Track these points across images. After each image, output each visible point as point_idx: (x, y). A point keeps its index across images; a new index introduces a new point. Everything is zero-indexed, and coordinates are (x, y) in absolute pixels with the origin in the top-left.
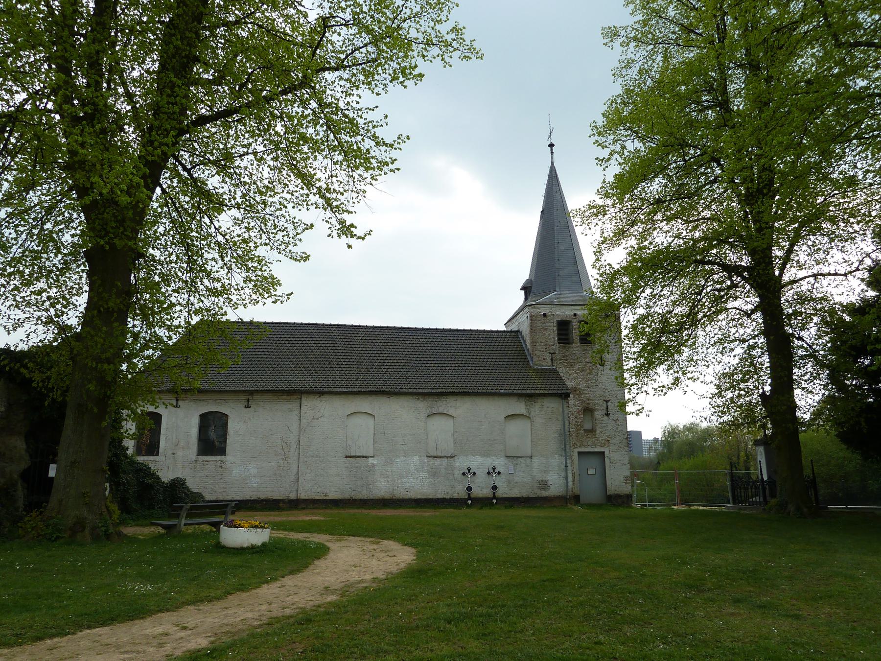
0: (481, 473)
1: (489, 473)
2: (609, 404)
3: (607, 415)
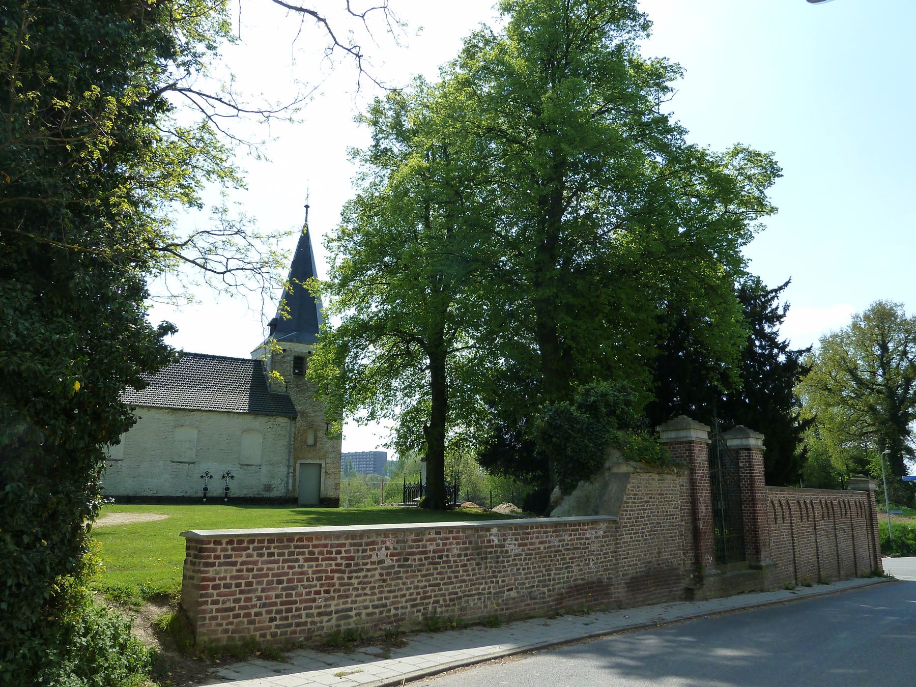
0: (217, 477)
1: (223, 477)
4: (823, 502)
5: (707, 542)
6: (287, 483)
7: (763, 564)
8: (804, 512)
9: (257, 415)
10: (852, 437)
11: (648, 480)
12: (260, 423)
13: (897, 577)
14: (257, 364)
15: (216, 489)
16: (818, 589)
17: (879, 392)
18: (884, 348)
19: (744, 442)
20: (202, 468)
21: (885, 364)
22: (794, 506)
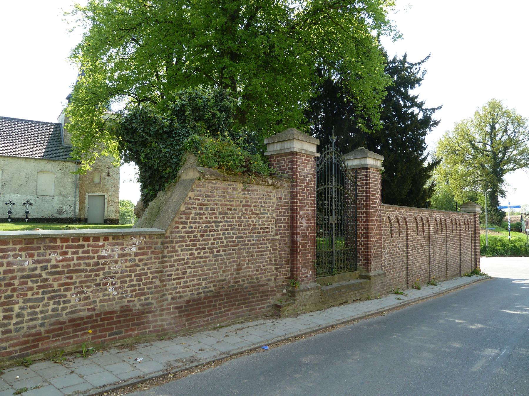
0: (19, 204)
1: (24, 204)
2: (110, 169)
3: (109, 175)
4: (438, 219)
5: (307, 255)
6: (75, 208)
7: (372, 274)
8: (420, 227)
9: (49, 160)
10: (470, 184)
11: (226, 189)
12: (51, 166)
13: (489, 275)
14: (58, 126)
15: (18, 212)
16: (427, 291)
17: (488, 155)
18: (493, 127)
19: (363, 162)
20: (7, 197)
21: (492, 138)
22: (411, 223)
